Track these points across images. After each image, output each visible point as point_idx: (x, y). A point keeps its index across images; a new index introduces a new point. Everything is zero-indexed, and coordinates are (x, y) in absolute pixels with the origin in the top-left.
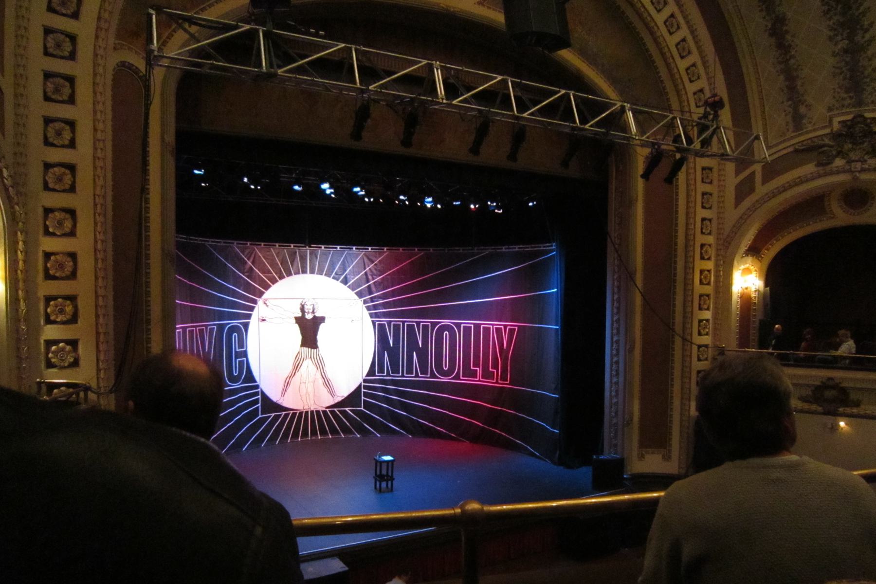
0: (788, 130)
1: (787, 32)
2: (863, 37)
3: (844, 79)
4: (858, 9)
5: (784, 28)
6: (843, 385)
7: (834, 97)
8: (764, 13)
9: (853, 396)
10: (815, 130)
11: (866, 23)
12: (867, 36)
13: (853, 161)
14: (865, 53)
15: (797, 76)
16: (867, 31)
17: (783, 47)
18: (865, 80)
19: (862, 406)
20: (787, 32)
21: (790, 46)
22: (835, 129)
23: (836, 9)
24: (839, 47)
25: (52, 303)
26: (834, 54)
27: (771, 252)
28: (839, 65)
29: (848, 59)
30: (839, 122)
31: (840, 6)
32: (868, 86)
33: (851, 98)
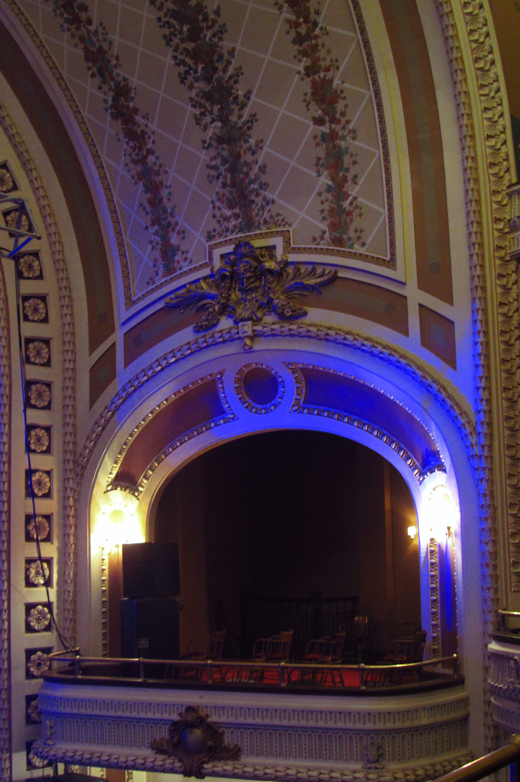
0: (157, 274)
1: (136, 111)
2: (240, 117)
3: (224, 185)
4: (225, 71)
5: (131, 105)
6: (213, 718)
7: (214, 216)
8: (98, 80)
9: (229, 739)
10: (191, 271)
11: (241, 93)
12: (246, 113)
13: (242, 320)
14: (246, 141)
15: (161, 182)
16: (244, 105)
17: (136, 137)
18: (252, 186)
19: (244, 760)
20: (136, 111)
21: (143, 133)
22: (216, 268)
23: (196, 72)
24: (210, 133)
25: (46, 609)
26: (206, 146)
27: (151, 484)
28: (213, 163)
29: (225, 153)
30: (222, 256)
31: (200, 66)
32: (257, 195)
33: (237, 216)
